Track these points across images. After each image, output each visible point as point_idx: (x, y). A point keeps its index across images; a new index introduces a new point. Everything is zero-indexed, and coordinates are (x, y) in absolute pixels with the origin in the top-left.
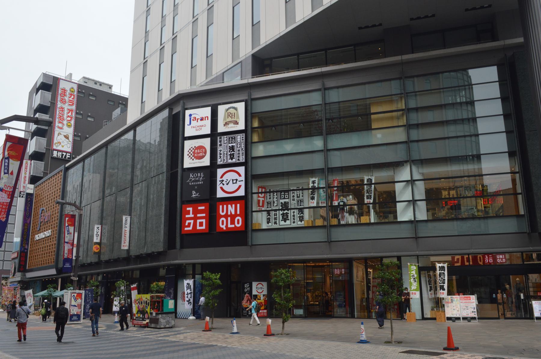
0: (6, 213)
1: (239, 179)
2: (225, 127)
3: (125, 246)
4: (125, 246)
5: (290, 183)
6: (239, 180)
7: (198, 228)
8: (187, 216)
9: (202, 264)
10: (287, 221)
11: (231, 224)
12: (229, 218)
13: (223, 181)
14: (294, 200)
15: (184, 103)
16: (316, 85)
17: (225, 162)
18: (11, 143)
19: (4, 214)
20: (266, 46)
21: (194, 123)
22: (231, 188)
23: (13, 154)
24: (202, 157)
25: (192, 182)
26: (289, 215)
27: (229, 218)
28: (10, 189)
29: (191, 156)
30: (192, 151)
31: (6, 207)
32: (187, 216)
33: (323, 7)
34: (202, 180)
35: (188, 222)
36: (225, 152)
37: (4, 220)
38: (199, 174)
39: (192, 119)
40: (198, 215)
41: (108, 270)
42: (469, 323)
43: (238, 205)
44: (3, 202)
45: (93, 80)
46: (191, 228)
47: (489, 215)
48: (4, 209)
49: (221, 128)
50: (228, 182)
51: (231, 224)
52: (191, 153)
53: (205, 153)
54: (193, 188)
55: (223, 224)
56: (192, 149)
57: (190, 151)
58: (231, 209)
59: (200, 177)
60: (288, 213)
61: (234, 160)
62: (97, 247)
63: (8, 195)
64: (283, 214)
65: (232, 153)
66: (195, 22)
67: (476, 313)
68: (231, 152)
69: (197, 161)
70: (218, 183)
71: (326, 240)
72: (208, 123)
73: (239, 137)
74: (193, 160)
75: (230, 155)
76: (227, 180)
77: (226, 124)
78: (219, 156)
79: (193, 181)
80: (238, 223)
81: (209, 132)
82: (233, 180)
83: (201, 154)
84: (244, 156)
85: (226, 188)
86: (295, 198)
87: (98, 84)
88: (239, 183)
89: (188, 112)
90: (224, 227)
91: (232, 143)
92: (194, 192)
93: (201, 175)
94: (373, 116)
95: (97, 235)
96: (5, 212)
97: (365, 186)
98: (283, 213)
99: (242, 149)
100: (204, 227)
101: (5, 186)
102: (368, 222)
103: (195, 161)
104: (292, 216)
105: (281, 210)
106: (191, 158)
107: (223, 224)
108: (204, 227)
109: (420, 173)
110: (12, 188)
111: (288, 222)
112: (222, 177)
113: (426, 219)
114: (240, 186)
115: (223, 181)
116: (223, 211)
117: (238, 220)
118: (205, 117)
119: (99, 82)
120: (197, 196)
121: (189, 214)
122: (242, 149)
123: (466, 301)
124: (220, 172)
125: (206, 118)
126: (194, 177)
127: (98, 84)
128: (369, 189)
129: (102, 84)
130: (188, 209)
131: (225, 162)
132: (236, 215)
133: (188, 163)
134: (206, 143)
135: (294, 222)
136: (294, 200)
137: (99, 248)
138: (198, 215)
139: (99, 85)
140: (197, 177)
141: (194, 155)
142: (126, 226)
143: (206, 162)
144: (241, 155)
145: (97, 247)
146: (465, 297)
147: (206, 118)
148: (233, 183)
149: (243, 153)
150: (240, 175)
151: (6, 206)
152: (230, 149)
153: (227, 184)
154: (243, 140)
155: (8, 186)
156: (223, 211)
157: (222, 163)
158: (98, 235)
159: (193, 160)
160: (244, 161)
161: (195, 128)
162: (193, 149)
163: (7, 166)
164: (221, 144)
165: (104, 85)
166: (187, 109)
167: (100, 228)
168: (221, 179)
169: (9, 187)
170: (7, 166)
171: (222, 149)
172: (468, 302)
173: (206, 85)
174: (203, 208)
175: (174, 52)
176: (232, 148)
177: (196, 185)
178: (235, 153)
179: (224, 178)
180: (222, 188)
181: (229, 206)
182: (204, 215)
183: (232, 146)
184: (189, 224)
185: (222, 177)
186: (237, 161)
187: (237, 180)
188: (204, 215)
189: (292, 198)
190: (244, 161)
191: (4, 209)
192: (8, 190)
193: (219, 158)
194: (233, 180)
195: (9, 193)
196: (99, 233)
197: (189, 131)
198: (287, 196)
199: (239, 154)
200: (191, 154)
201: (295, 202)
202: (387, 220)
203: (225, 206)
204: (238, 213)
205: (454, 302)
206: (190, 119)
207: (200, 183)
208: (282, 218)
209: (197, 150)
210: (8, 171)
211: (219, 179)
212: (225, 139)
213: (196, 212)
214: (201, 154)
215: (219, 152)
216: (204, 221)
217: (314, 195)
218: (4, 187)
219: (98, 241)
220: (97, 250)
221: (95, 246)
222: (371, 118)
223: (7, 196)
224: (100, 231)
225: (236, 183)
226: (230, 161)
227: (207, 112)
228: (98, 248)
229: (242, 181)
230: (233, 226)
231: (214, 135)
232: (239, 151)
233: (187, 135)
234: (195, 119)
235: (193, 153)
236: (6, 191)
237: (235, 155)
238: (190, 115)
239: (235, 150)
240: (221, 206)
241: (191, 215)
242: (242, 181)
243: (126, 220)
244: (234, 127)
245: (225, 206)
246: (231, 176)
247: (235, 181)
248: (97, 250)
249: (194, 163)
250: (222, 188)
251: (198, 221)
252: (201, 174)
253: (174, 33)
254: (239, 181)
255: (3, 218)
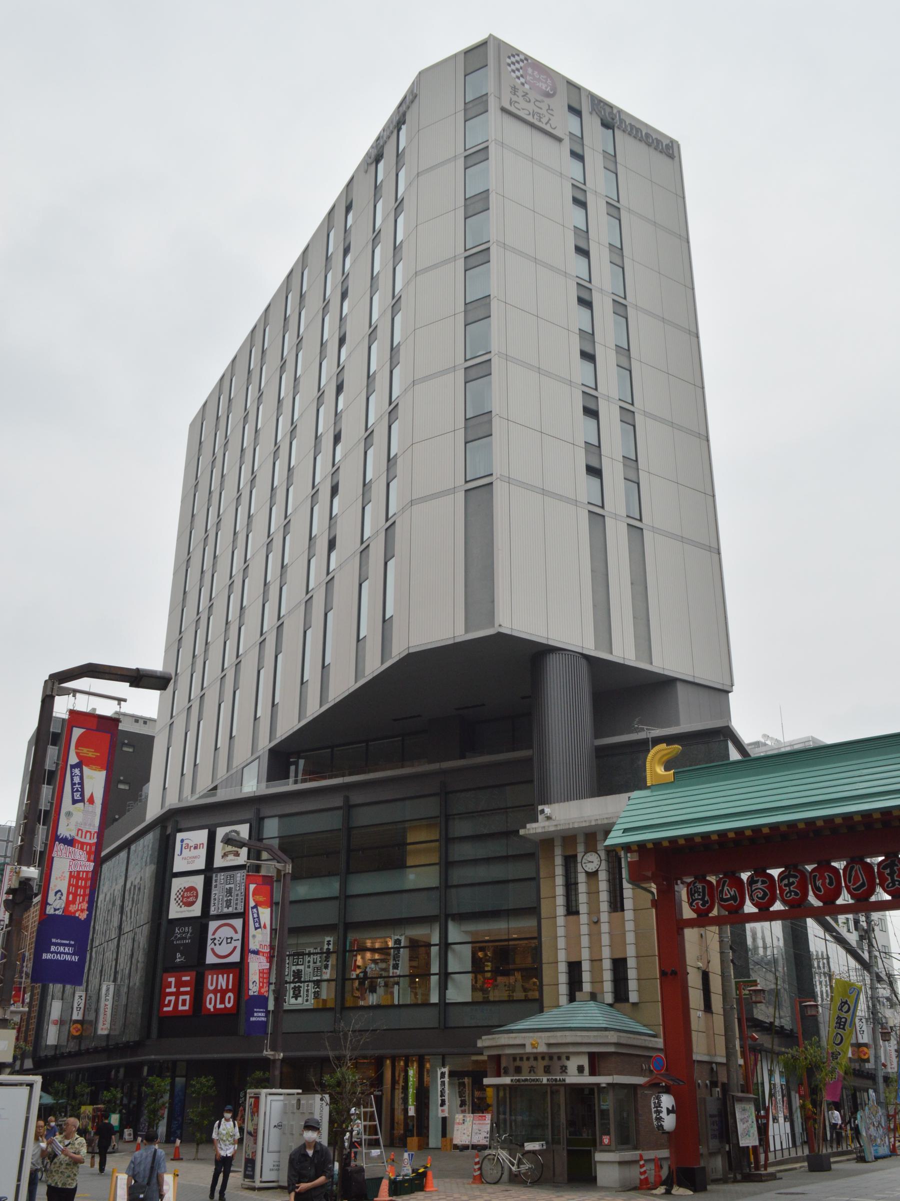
0: (87, 899)
1: (236, 936)
2: (222, 860)
3: (103, 1029)
4: (103, 1029)
5: (299, 942)
6: (234, 939)
7: (181, 1008)
8: (168, 990)
9: (189, 1062)
10: (299, 998)
11: (220, 1004)
12: (219, 995)
13: (215, 939)
14: (309, 967)
15: (177, 822)
16: (338, 801)
17: (220, 911)
18: (83, 730)
19: (83, 900)
20: (374, 678)
21: (186, 852)
22: (223, 950)
23: (90, 755)
24: (191, 904)
25: (177, 940)
26: (302, 989)
27: (219, 995)
28: (90, 839)
29: (179, 901)
30: (180, 894)
31: (86, 884)
32: (168, 990)
33: (364, 679)
34: (190, 938)
35: (168, 998)
36: (221, 897)
37: (83, 916)
38: (187, 928)
39: (184, 846)
40: (182, 989)
41: (67, 1067)
42: (462, 1153)
43: (231, 975)
44: (78, 872)
45: (132, 716)
46: (170, 1009)
47: (751, 979)
48: (81, 887)
49: (218, 862)
50: (221, 940)
51: (220, 1004)
52: (180, 896)
53: (197, 897)
54: (177, 948)
55: (211, 1003)
56: (180, 891)
57: (178, 894)
58: (222, 981)
59: (188, 932)
60: (301, 987)
61: (230, 910)
62: (77, 1027)
63: (89, 853)
64: (294, 988)
65: (229, 898)
66: (308, 602)
67: (488, 1140)
68: (228, 897)
69: (186, 908)
70: (209, 942)
71: (437, 1025)
72: (203, 852)
73: (239, 875)
74: (181, 907)
75: (227, 901)
76: (220, 938)
77: (225, 855)
78: (212, 902)
79: (180, 939)
80: (229, 1002)
81: (203, 867)
82: (227, 938)
83: (191, 899)
84: (243, 904)
85: (218, 950)
86: (311, 964)
87: (141, 722)
88: (234, 943)
89: (180, 836)
90: (211, 1007)
91: (230, 884)
92: (178, 955)
93: (188, 929)
94: (409, 847)
95: (78, 1009)
96: (84, 896)
97: (392, 950)
98: (295, 986)
99: (242, 893)
100: (187, 1008)
101: (80, 832)
102: (390, 1003)
103: (184, 908)
104: (305, 991)
105: (293, 982)
106: (179, 904)
107: (211, 1003)
108: (187, 1008)
109: (463, 931)
110: (96, 835)
111: (300, 1000)
112: (214, 934)
113: (470, 1000)
114: (235, 948)
115: (215, 939)
116: (212, 985)
117: (230, 998)
118: (200, 844)
119: (142, 718)
120: (182, 961)
121: (170, 987)
122: (242, 893)
123: (481, 1122)
124: (213, 925)
125: (201, 845)
126: (180, 933)
127: (141, 722)
128: (396, 954)
129: (148, 722)
130: (170, 979)
131: (220, 911)
132: (227, 990)
133: (176, 911)
134: (198, 882)
135: (307, 1001)
136: (309, 967)
137: (81, 1029)
138: (182, 989)
139: (142, 722)
140: (184, 932)
141: (183, 899)
142: (107, 998)
143: (196, 910)
144: (239, 901)
145: (77, 1027)
146: (480, 1116)
147: (201, 845)
148: (227, 943)
149: (242, 899)
150: (236, 932)
151: (86, 880)
152: (227, 892)
153: (220, 944)
154: (243, 879)
155: (87, 832)
156: (212, 985)
157: (215, 913)
158: (80, 1008)
159: (181, 907)
160: (242, 911)
161: (187, 861)
162: (182, 891)
163: (79, 784)
164: (217, 885)
165: (151, 722)
166: (180, 831)
167: (83, 998)
168: (213, 937)
169: (88, 835)
170: (79, 784)
171: (217, 892)
172: (483, 1124)
173: (206, 797)
174: (188, 978)
175: (329, 609)
176: (229, 891)
177: (181, 945)
178: (232, 898)
179: (217, 936)
180: (212, 950)
181: (220, 976)
182: (188, 989)
183: (230, 888)
184: (170, 1001)
185: (214, 934)
186: (235, 911)
187: (232, 938)
188: (188, 989)
189: (307, 964)
190: (242, 911)
191: (81, 887)
192: (87, 840)
193: (212, 905)
194: (227, 938)
195: (90, 849)
196: (82, 1006)
197: (179, 865)
198: (301, 961)
199: (237, 900)
200: (179, 899)
201: (311, 970)
202: (70, 1038)
203: (215, 976)
204: (230, 987)
205: (466, 1123)
206: (182, 845)
207: (187, 941)
208: (293, 994)
209: (187, 892)
210: (82, 795)
211: (210, 936)
212: (222, 877)
213: (179, 984)
214: (191, 898)
215: (213, 896)
216: (187, 997)
217: (328, 961)
218: (77, 835)
219: (80, 1017)
220: (77, 1031)
221: (74, 1026)
222: (406, 848)
223: (86, 856)
224: (83, 1001)
225: (231, 943)
226: (226, 910)
227: (201, 836)
228: (79, 1030)
229: (238, 940)
230: (222, 1006)
231: (209, 871)
232: (237, 895)
233: (176, 869)
234: (188, 846)
235: (182, 896)
236: (83, 844)
237: (232, 901)
238: (182, 841)
239: (233, 894)
240: (210, 977)
241: (173, 989)
242: (238, 940)
243: (108, 990)
244: (234, 860)
245: (215, 976)
246: (226, 932)
247: (229, 941)
248: (77, 1031)
249: (182, 912)
250: (212, 950)
251: (181, 998)
252: (189, 929)
253: (390, 516)
254: (235, 940)
255: (82, 911)
